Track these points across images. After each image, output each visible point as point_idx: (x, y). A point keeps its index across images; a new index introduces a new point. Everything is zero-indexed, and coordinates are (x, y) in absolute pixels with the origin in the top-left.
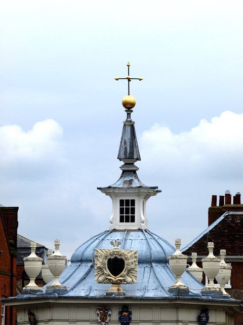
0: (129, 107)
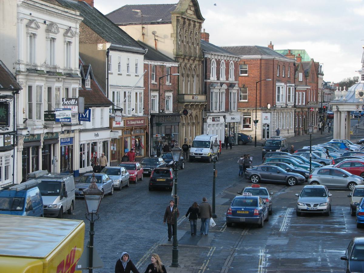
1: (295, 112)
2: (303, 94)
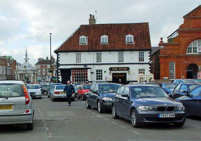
0: (26, 50)
1: (6, 77)
2: (10, 71)
